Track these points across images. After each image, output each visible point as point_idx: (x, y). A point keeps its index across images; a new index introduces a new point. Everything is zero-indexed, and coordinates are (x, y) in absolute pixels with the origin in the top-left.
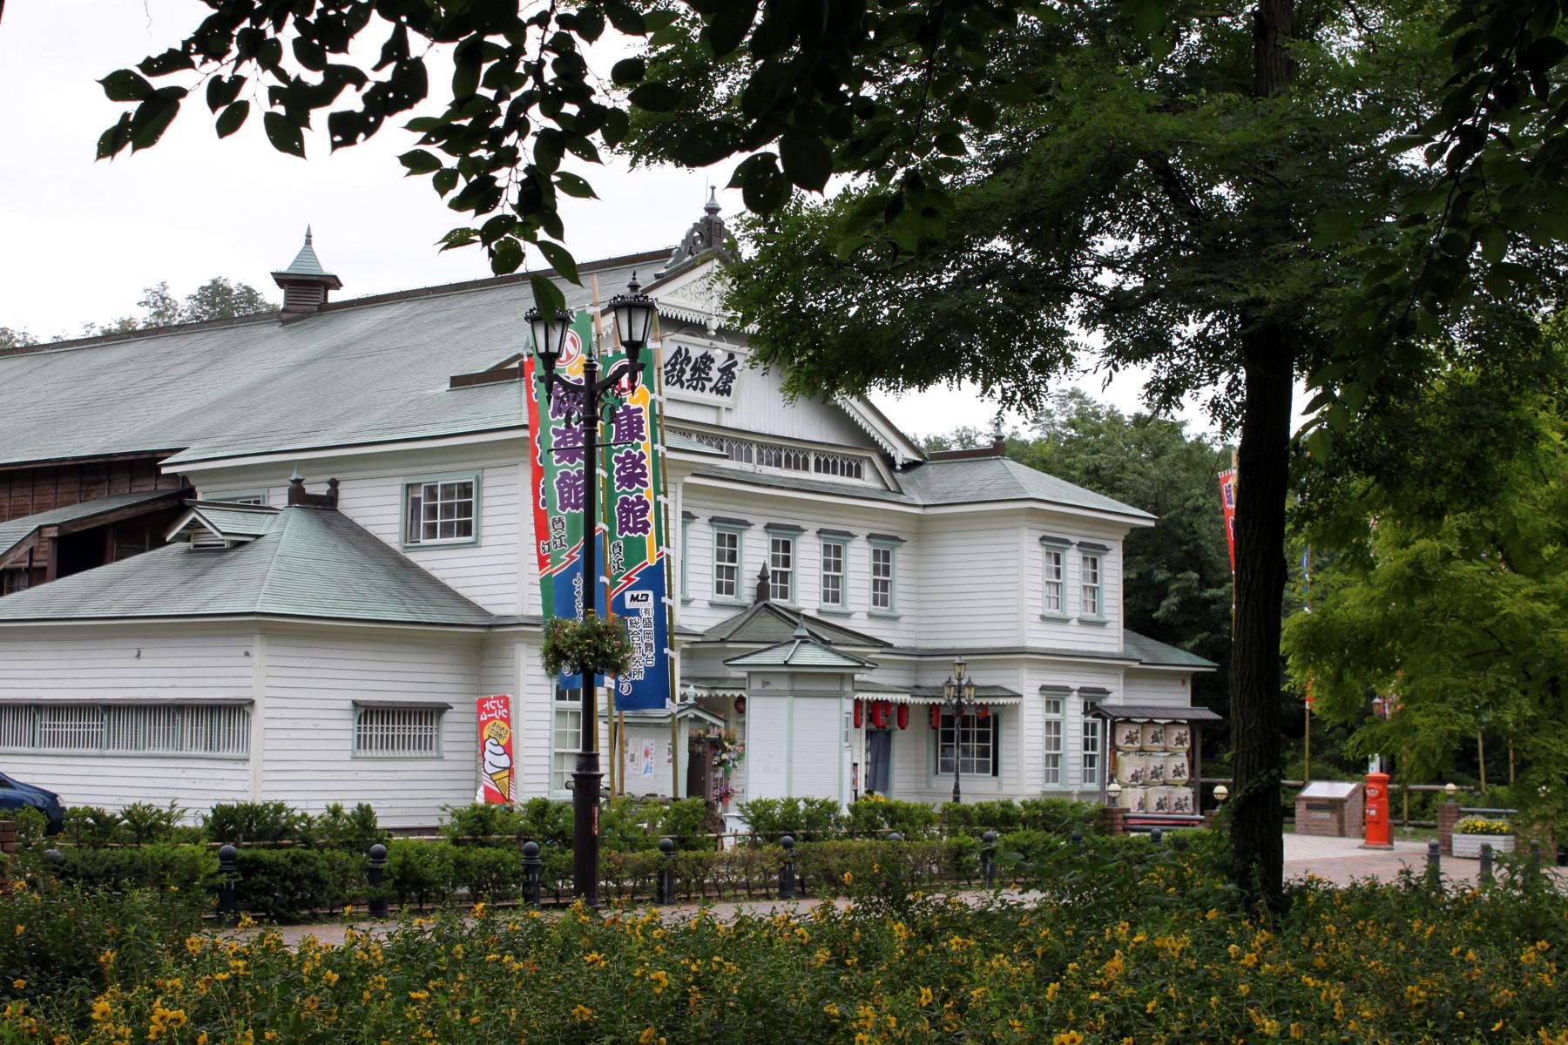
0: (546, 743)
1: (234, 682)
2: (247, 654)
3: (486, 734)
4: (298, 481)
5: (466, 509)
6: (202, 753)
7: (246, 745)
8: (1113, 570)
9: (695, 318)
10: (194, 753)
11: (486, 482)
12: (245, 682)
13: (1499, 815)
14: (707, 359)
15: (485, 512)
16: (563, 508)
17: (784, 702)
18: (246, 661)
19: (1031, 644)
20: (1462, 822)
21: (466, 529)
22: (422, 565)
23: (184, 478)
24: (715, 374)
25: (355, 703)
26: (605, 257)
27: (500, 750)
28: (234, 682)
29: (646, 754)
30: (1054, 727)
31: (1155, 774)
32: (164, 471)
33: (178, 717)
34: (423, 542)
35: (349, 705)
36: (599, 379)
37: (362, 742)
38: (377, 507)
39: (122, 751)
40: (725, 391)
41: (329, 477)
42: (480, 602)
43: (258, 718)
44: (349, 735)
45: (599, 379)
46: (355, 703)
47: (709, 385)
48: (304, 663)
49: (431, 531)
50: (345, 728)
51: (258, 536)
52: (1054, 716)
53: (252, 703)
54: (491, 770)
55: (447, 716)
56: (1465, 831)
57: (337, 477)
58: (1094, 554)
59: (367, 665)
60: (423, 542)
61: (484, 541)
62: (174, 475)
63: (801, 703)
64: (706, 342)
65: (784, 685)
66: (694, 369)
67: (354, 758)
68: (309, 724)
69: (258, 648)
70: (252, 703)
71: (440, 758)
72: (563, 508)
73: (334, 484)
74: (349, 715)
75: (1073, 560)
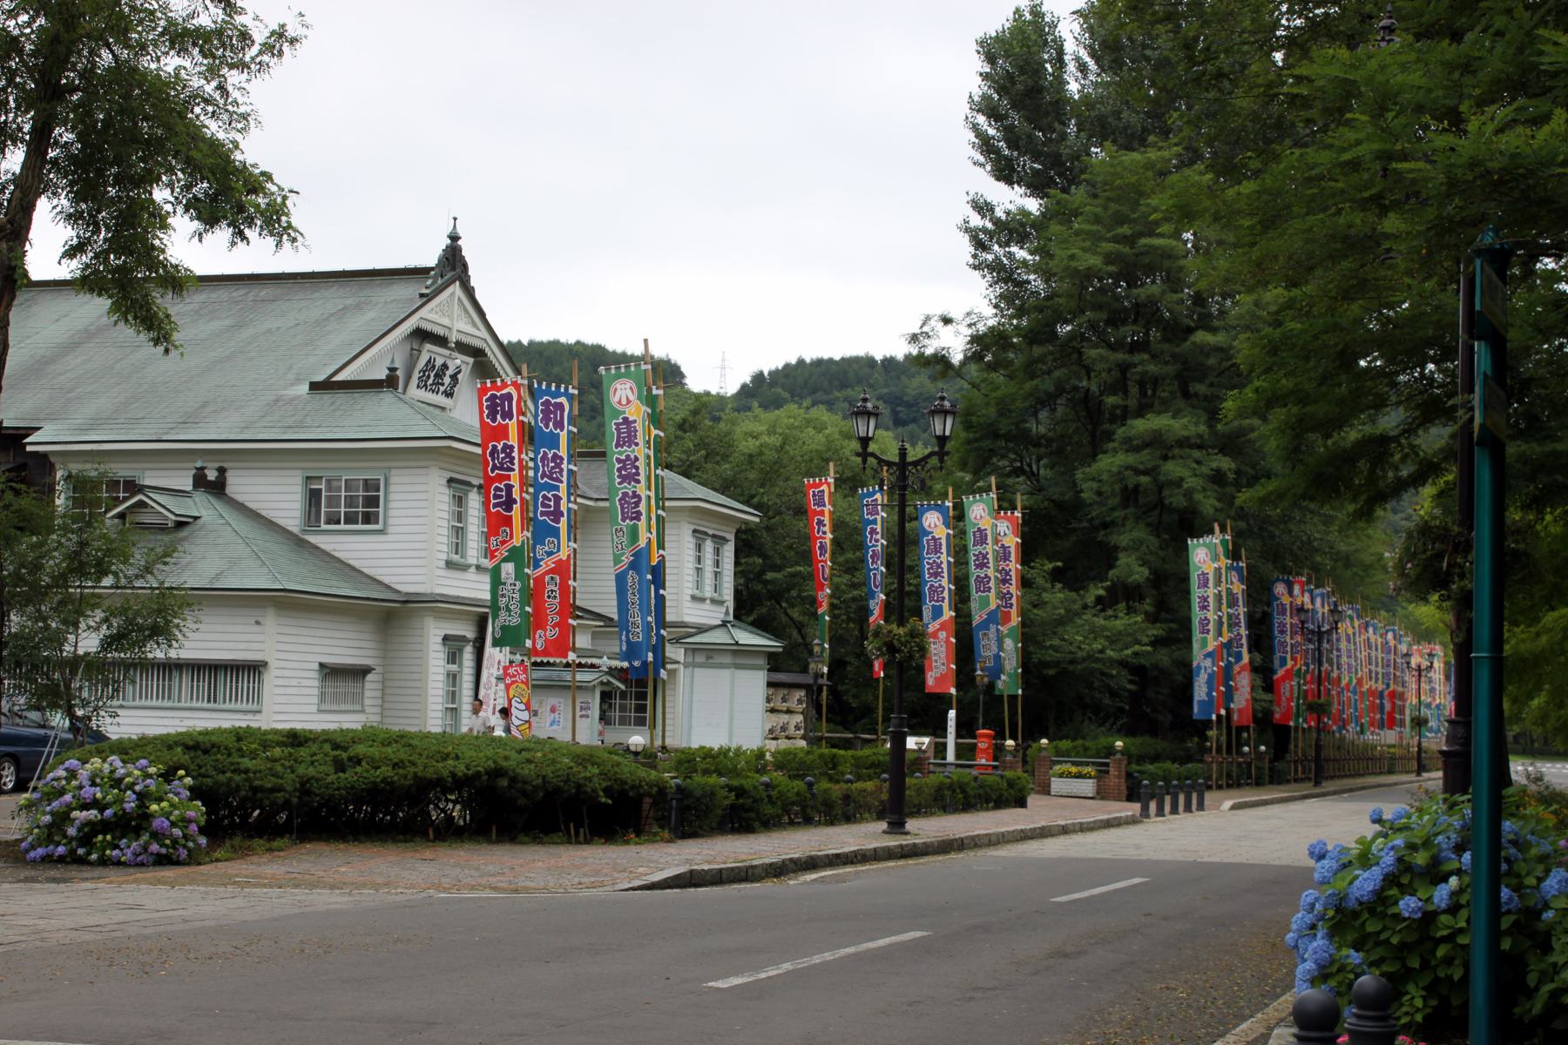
0: (440, 700)
1: (243, 646)
2: (258, 623)
3: (512, 693)
4: (203, 468)
5: (373, 502)
6: (205, 705)
7: (258, 697)
8: (729, 551)
9: (440, 331)
10: (194, 704)
11: (393, 480)
12: (259, 646)
13: (1087, 764)
14: (445, 366)
15: (392, 505)
16: (624, 520)
17: (726, 673)
18: (256, 628)
19: (687, 619)
20: (1057, 768)
21: (368, 518)
22: (323, 546)
23: (45, 455)
24: (447, 380)
25: (322, 665)
26: (340, 269)
27: (522, 707)
28: (243, 646)
29: (553, 710)
30: (453, 678)
31: (784, 729)
32: (29, 448)
33: (176, 674)
34: (324, 527)
35: (316, 666)
36: (909, 459)
37: (322, 697)
38: (278, 496)
39: (154, 703)
40: (449, 394)
41: (217, 465)
42: (386, 580)
43: (269, 679)
44: (316, 691)
45: (909, 459)
46: (322, 665)
47: (442, 389)
48: (294, 630)
49: (333, 519)
50: (313, 682)
51: (196, 518)
52: (454, 667)
53: (265, 664)
54: (517, 722)
55: (369, 677)
56: (1061, 776)
57: (225, 465)
58: (719, 540)
59: (337, 634)
60: (324, 527)
61: (390, 529)
62: (36, 453)
63: (740, 674)
64: (447, 352)
65: (728, 659)
66: (436, 376)
67: (319, 711)
68: (294, 682)
69: (271, 619)
70: (265, 664)
71: (363, 711)
72: (624, 520)
73: (222, 471)
74: (315, 675)
75: (709, 546)
